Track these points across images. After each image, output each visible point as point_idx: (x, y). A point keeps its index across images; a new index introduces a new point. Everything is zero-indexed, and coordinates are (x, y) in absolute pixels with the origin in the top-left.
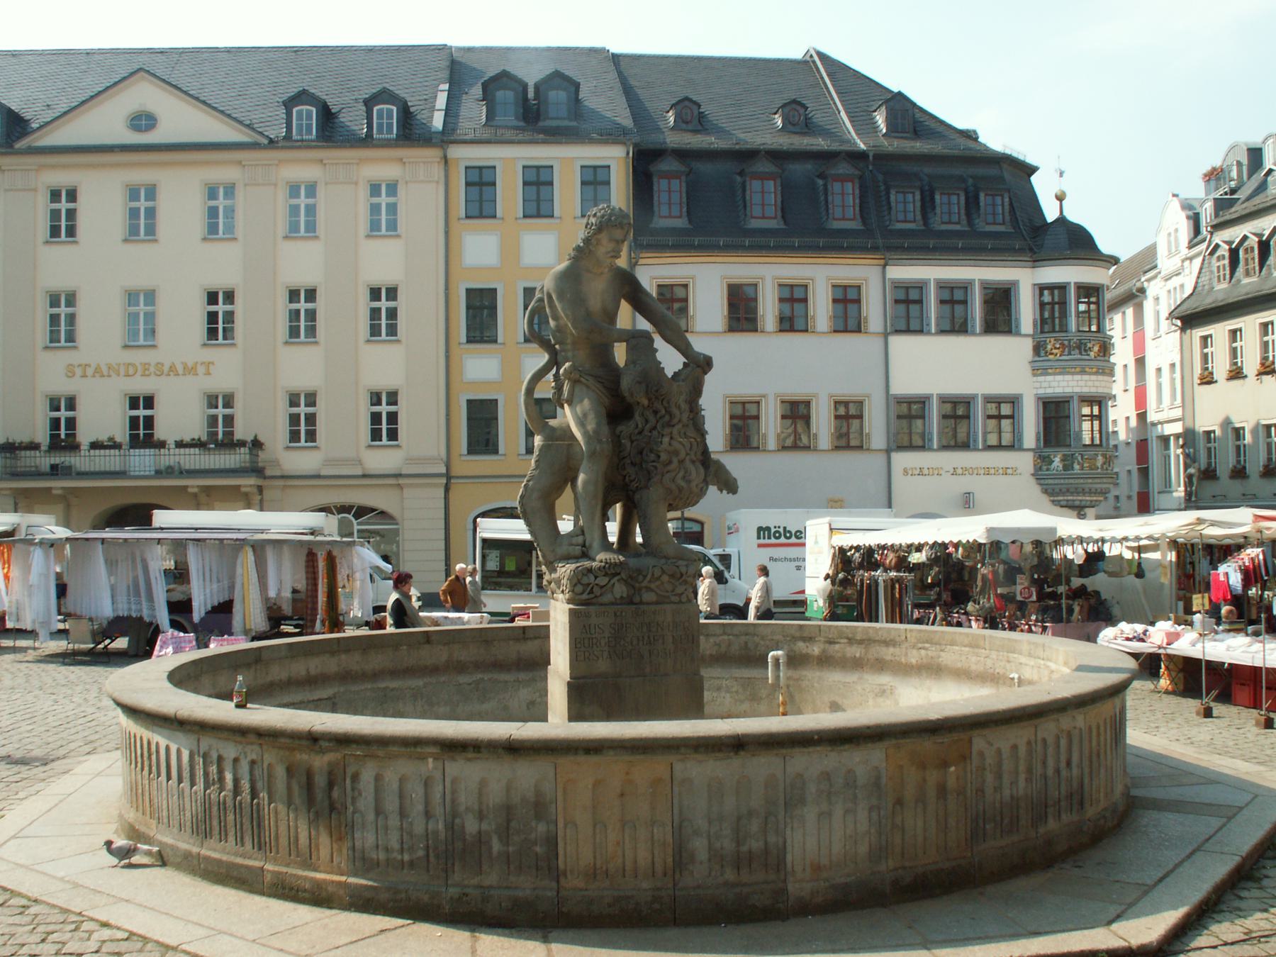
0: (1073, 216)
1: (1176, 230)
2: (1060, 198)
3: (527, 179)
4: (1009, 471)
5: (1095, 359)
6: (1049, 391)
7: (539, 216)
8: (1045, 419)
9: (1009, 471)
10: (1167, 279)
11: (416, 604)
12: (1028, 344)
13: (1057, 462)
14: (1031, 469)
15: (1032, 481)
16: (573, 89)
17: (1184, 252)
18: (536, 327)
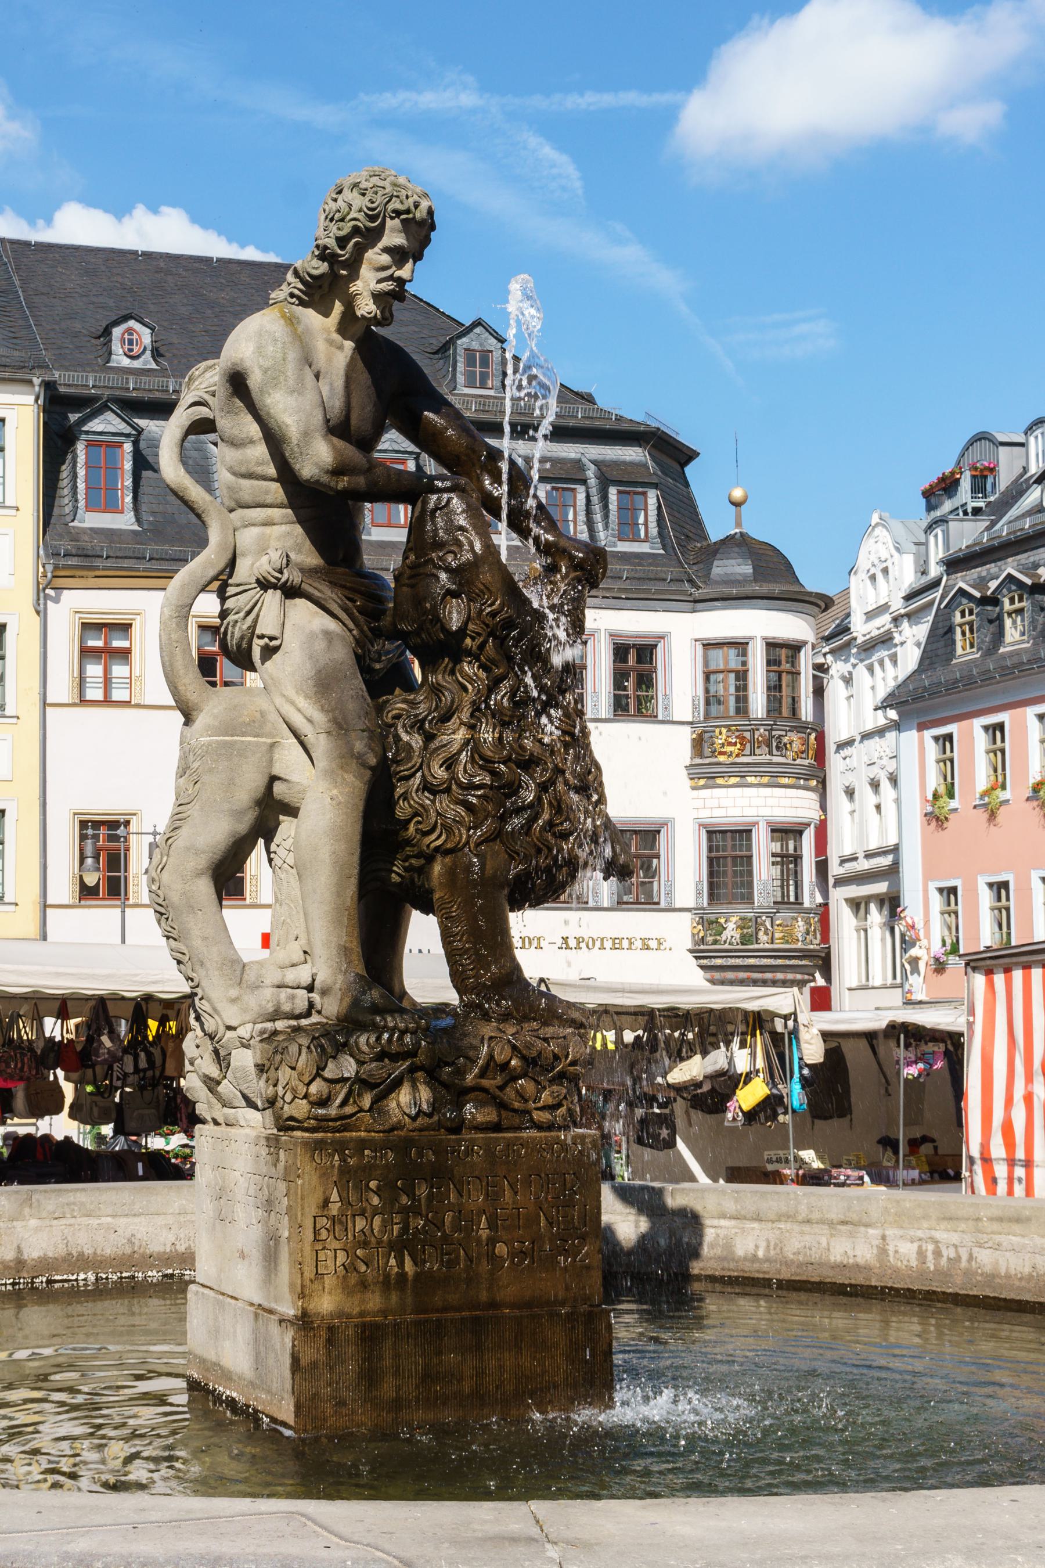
6: (717, 813)
8: (711, 861)
9: (653, 944)
11: (536, 476)
12: (685, 736)
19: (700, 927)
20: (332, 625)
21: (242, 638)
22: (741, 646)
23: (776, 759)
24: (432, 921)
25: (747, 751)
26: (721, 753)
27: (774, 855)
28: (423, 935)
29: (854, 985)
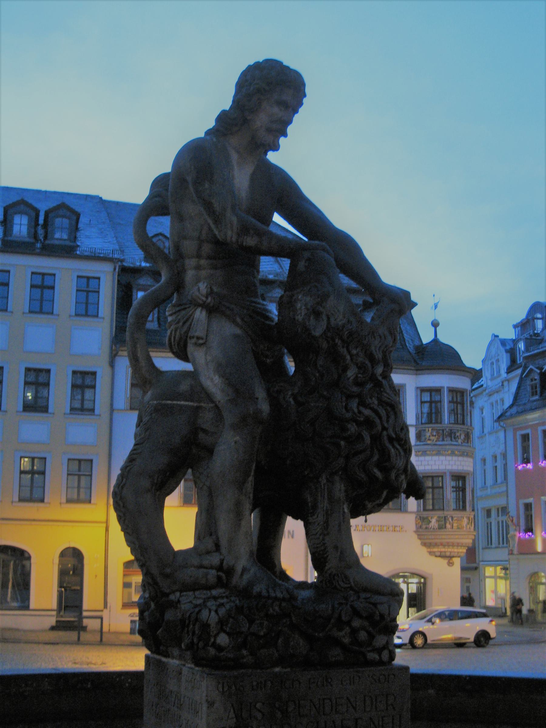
0: (443, 339)
1: (498, 361)
2: (435, 325)
3: (51, 291)
4: (397, 529)
5: (461, 445)
7: (41, 312)
10: (490, 395)
13: (434, 523)
14: (414, 528)
15: (415, 536)
16: (75, 218)
17: (504, 375)
18: (434, 452)
19: (419, 521)
20: (238, 331)
21: (181, 338)
22: (438, 390)
23: (453, 443)
24: (300, 524)
25: (441, 439)
26: (429, 440)
27: (453, 487)
28: (294, 531)
29: (77, 467)
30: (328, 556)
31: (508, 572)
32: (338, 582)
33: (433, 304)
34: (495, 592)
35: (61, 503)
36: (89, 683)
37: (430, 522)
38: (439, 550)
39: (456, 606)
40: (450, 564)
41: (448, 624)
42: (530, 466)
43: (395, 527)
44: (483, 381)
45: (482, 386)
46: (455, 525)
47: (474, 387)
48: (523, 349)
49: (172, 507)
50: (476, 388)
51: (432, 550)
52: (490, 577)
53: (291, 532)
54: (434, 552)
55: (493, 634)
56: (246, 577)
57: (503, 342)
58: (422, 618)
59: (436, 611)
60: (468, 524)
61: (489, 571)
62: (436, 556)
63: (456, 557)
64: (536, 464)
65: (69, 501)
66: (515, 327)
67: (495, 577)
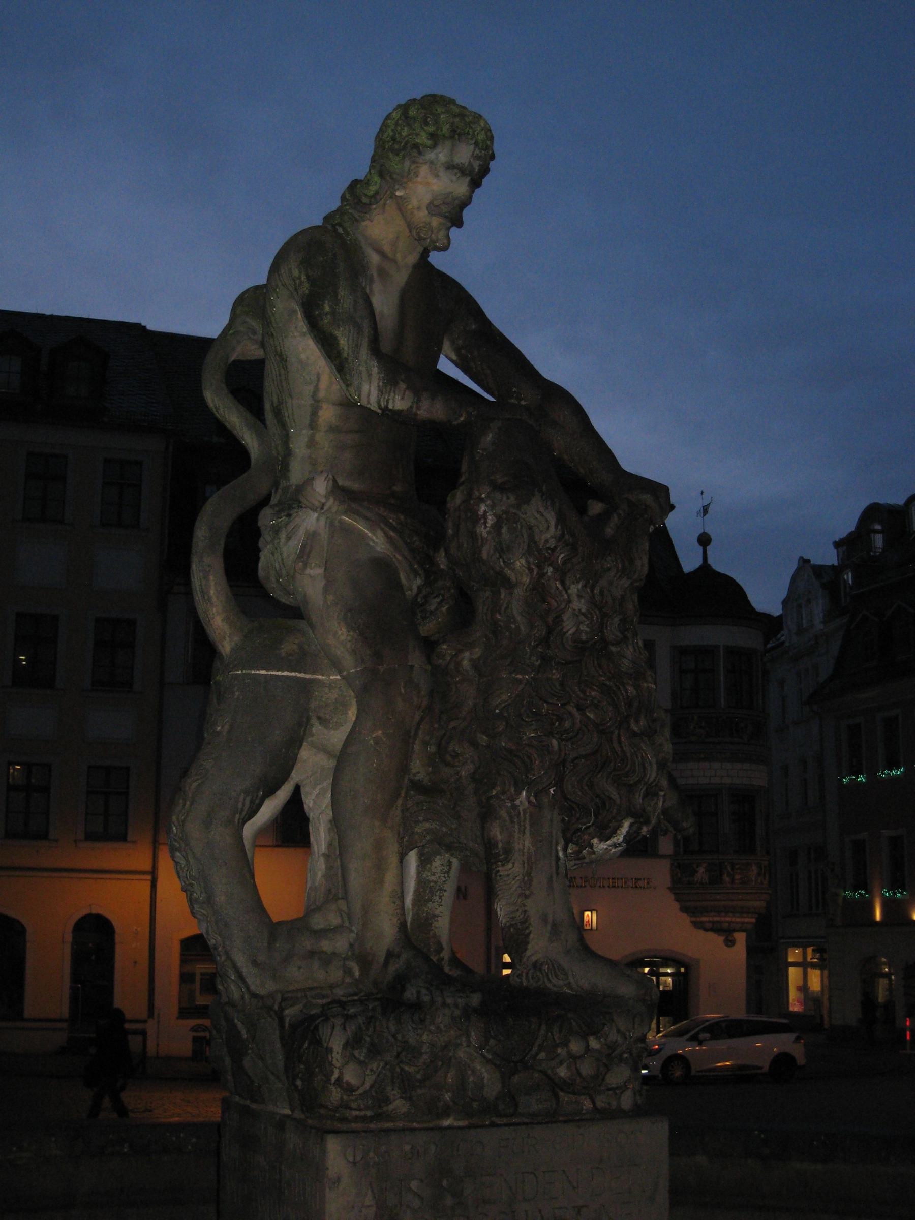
0: (719, 564)
2: (704, 540)
4: (641, 883)
22: (709, 651)
30: (530, 933)
31: (825, 956)
32: (547, 975)
33: (701, 506)
34: (804, 988)
35: (75, 841)
36: (126, 1145)
37: (697, 872)
38: (711, 919)
39: (739, 1012)
40: (730, 943)
41: (723, 1044)
42: (861, 778)
43: (637, 880)
44: (784, 636)
45: (782, 643)
46: (737, 877)
47: (769, 646)
48: (850, 582)
49: (266, 846)
50: (773, 648)
51: (698, 919)
52: (794, 964)
53: (463, 889)
54: (702, 922)
55: (801, 1060)
56: (392, 968)
57: (819, 571)
58: (679, 1034)
59: (707, 1021)
60: (759, 875)
61: (794, 954)
62: (706, 930)
63: (737, 931)
64: (872, 776)
65: (91, 837)
66: (837, 545)
67: (804, 965)
